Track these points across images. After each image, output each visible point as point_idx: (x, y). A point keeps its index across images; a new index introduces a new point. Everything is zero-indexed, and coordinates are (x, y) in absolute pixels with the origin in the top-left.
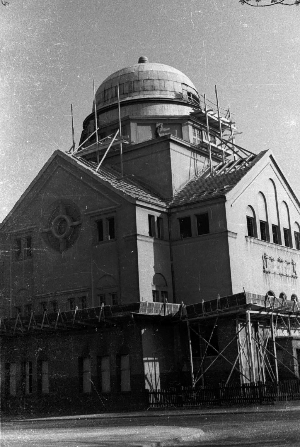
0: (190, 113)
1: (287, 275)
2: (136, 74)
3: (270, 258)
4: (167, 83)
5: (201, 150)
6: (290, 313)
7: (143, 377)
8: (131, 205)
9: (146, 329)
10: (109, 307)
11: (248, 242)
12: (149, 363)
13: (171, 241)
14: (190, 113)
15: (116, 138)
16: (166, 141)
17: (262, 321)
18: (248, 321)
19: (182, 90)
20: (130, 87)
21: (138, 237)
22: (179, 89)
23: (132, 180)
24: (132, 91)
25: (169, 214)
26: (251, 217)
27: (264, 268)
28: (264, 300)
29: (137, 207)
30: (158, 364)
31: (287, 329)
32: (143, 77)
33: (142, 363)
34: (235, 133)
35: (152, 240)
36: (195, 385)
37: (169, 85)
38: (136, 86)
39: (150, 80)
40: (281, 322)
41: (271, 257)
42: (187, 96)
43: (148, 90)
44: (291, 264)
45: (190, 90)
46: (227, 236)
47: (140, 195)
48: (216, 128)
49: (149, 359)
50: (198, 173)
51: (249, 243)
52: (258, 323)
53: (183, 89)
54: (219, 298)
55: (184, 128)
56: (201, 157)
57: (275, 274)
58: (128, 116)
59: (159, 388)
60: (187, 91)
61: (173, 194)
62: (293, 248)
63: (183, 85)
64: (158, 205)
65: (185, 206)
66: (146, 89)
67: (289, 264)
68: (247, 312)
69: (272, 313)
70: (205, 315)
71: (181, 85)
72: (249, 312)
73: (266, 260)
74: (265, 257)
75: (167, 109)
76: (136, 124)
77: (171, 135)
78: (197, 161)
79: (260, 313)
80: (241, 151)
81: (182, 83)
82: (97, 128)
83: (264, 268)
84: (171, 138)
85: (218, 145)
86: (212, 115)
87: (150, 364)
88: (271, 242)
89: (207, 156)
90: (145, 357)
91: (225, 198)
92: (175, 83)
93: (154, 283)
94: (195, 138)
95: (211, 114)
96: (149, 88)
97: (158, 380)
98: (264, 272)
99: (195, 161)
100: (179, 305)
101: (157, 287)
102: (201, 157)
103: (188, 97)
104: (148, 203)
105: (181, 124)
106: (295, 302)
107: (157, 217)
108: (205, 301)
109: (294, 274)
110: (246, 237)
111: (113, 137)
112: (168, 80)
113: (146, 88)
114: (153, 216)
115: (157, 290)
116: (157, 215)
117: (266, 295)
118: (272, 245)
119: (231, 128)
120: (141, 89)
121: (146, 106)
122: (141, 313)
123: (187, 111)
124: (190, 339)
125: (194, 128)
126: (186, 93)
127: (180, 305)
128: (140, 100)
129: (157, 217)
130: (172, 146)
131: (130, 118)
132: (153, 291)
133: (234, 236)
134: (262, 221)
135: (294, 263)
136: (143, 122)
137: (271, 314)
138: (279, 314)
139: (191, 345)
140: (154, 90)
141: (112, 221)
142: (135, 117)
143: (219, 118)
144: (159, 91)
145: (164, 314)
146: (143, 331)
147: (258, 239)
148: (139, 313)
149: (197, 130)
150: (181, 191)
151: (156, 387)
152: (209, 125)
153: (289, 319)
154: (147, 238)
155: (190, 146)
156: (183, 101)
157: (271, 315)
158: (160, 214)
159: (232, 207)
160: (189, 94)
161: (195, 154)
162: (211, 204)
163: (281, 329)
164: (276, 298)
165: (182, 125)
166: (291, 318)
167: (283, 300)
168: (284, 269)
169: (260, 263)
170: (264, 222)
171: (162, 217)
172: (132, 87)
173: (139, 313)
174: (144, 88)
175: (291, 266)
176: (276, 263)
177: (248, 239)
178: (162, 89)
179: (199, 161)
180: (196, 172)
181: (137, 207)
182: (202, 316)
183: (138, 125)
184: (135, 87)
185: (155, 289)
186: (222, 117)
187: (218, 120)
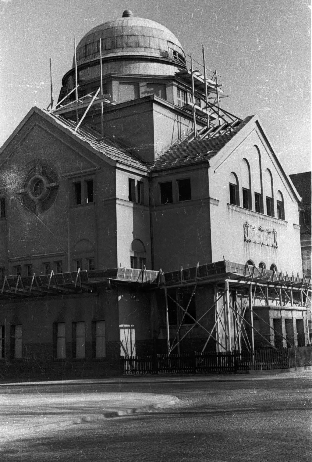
4: (152, 39)
6: (269, 283)
10: (86, 272)
13: (151, 206)
16: (150, 101)
17: (239, 290)
20: (113, 42)
21: (117, 202)
22: (165, 47)
25: (149, 179)
27: (245, 237)
29: (117, 170)
30: (133, 331)
31: (265, 299)
35: (132, 205)
37: (154, 43)
40: (259, 292)
42: (173, 55)
43: (131, 47)
44: (272, 233)
48: (201, 90)
51: (230, 211)
52: (237, 292)
55: (168, 89)
56: (185, 120)
57: (255, 243)
58: (110, 74)
59: (134, 355)
68: (226, 280)
72: (228, 281)
74: (246, 226)
81: (169, 41)
83: (245, 237)
84: (155, 99)
86: (198, 76)
87: (126, 331)
89: (191, 119)
91: (208, 163)
92: (161, 41)
96: (133, 45)
98: (245, 240)
100: (157, 272)
101: (135, 253)
102: (185, 120)
104: (129, 166)
106: (274, 272)
108: (184, 269)
111: (94, 95)
112: (153, 37)
116: (137, 178)
118: (254, 214)
120: (125, 45)
122: (118, 279)
123: (172, 71)
124: (167, 306)
125: (179, 89)
130: (155, 107)
132: (131, 257)
136: (126, 80)
139: (167, 313)
140: (139, 47)
141: (90, 184)
143: (205, 80)
144: (143, 48)
145: (141, 281)
146: (120, 298)
148: (116, 278)
151: (132, 354)
158: (141, 178)
160: (175, 53)
161: (179, 116)
167: (263, 269)
173: (117, 279)
175: (272, 235)
177: (230, 207)
179: (182, 124)
180: (179, 135)
181: (117, 170)
185: (133, 255)
187: (204, 82)
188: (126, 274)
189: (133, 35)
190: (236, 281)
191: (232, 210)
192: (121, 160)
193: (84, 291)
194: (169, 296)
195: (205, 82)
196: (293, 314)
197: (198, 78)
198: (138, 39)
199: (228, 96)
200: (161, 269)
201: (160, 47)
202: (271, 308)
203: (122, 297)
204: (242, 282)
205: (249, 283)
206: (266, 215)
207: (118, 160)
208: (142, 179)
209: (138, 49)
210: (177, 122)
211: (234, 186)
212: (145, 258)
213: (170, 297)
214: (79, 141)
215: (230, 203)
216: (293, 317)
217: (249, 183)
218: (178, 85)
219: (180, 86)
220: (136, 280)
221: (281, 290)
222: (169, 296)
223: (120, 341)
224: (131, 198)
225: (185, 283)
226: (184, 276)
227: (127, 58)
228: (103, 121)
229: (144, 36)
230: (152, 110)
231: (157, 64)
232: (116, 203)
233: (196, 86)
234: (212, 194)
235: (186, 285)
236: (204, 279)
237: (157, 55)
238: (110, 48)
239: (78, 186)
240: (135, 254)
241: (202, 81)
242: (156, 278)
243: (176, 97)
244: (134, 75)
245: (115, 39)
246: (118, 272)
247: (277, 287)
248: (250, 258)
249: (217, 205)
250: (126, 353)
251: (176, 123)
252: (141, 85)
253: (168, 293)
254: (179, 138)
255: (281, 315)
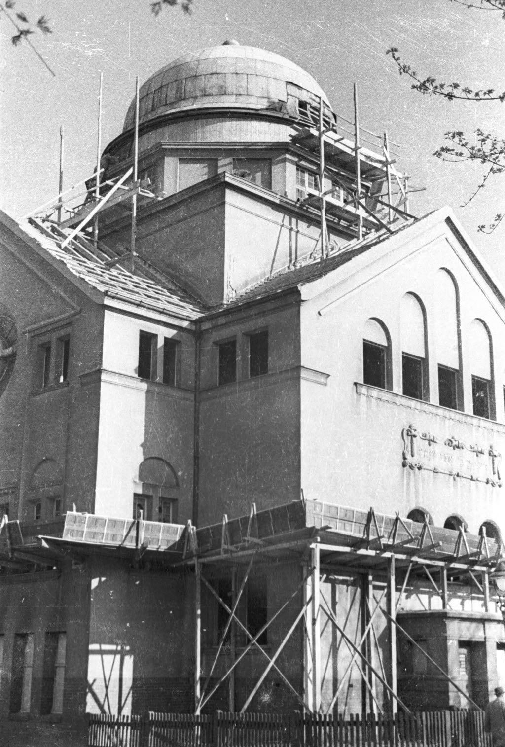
0: (291, 138)
1: (472, 476)
2: (193, 65)
3: (425, 436)
4: (253, 79)
5: (307, 211)
6: (449, 559)
7: (80, 686)
8: (90, 308)
9: (103, 579)
10: (16, 523)
11: (362, 396)
12: (105, 657)
13: (198, 391)
14: (291, 138)
15: (124, 184)
16: (216, 187)
17: (357, 568)
18: (314, 568)
19: (286, 94)
20: (178, 90)
21: (104, 376)
22: (279, 93)
23: (158, 271)
24: (181, 97)
25: (196, 332)
26: (484, 379)
27: (405, 458)
28: (365, 522)
29: (106, 312)
30: (129, 661)
31: (438, 594)
32: (203, 69)
33: (88, 652)
34: (411, 189)
35: (144, 386)
36: (202, 711)
37: (257, 86)
38: (189, 87)
39: (219, 74)
40: (417, 577)
41: (428, 435)
42: (298, 109)
43: (211, 95)
44: (486, 453)
45: (305, 97)
46: (298, 378)
47: (115, 287)
48: (342, 167)
49: (105, 647)
50: (299, 259)
51: (363, 399)
52: (370, 578)
53: (288, 95)
54: (254, 511)
55: (276, 169)
56: (308, 227)
57: (436, 472)
58: (160, 142)
59: (127, 711)
60: (298, 98)
61: (225, 297)
62: (431, 400)
63: (289, 86)
64: (165, 311)
65: (225, 315)
66: (207, 93)
67: (479, 454)
68: (313, 546)
69: (392, 554)
70: (226, 551)
71: (285, 86)
72: (317, 547)
73: (412, 440)
74: (409, 433)
75: (246, 130)
76: (176, 159)
77: (226, 174)
78: (299, 235)
79: (355, 551)
80: (403, 217)
81: (288, 83)
82: (101, 169)
83: (405, 458)
84: (227, 180)
85: (325, 194)
86: (336, 141)
87: (108, 658)
88: (431, 403)
89: (315, 222)
90: (93, 643)
91: (298, 293)
92: (273, 82)
93: (141, 477)
94: (301, 188)
95: (336, 139)
96: (215, 91)
97: (127, 697)
98: (404, 465)
99: (294, 234)
100: (180, 527)
101: (144, 486)
102: (308, 227)
103: (299, 110)
104: (139, 305)
105: (270, 159)
106: (460, 535)
107: (166, 339)
108: (231, 520)
109: (494, 478)
110: (356, 384)
111: (116, 182)
112: (257, 75)
113: (208, 91)
114: (155, 336)
115: (146, 492)
116: (163, 333)
117: (369, 510)
118: (434, 410)
119: (387, 172)
120: (199, 93)
121: (203, 126)
122: (67, 537)
123: (283, 134)
124: (198, 605)
125: (300, 168)
126: (296, 101)
127: (184, 526)
128: (190, 113)
129: (166, 339)
130: (231, 197)
131: (163, 147)
132: (136, 495)
133: (322, 380)
134: (368, 341)
135: (495, 453)
136: (188, 156)
137: (390, 556)
138: (415, 558)
139: (199, 621)
140: (225, 94)
141: (66, 342)
142: (174, 145)
143: (355, 150)
144: (235, 96)
145: (135, 544)
146: (95, 583)
147: (466, 412)
148: (61, 537)
149: (309, 174)
150: (247, 291)
151: (120, 708)
152: (325, 160)
153: (445, 572)
154: (131, 380)
155: (278, 202)
156: (280, 115)
157: (389, 560)
158: (174, 332)
159: (321, 317)
160: (303, 104)
161: (294, 220)
162: (274, 309)
163: (460, 597)
164: (401, 521)
165: (273, 161)
166: (450, 570)
167: (425, 526)
168: (466, 464)
169: (395, 446)
170: (420, 358)
171: (178, 339)
172: (181, 90)
173: (63, 539)
174: (205, 91)
175: (486, 457)
176: (440, 448)
177: (364, 390)
178: (242, 93)
179: (302, 234)
180: (294, 257)
181: (106, 312)
182: (219, 554)
183: (182, 161)
184: (188, 89)
185: (140, 491)
186: (361, 148)
187: (353, 154)
188: (89, 527)
189: (216, 74)
190: (347, 549)
191: (369, 397)
192: (113, 291)
193: (40, 569)
194: (204, 580)
195: (356, 153)
196: (486, 631)
197: (337, 145)
198: (225, 81)
199: (424, 189)
200: (190, 521)
201: (269, 93)
202: (448, 615)
203: (100, 580)
204: (362, 552)
205: (387, 554)
206: (471, 413)
207: (107, 291)
208: (177, 334)
209: (225, 98)
210: (288, 231)
211: (485, 384)
212: (177, 500)
213: (207, 584)
214: (49, 260)
215: (362, 382)
216: (485, 638)
217: (423, 346)
218: (300, 160)
219: (303, 163)
220: (120, 543)
221: (487, 576)
222: (204, 580)
223: (87, 682)
224: (144, 371)
225: (232, 552)
226: (232, 536)
227: (198, 115)
228: (135, 230)
229: (237, 74)
230: (224, 203)
231: (258, 122)
232: (99, 380)
233: (328, 157)
234: (309, 355)
235: (234, 555)
236: (270, 543)
237: (260, 105)
238: (173, 100)
239: (46, 348)
240: (143, 490)
241: (349, 151)
242: (177, 539)
243: (290, 181)
244: (210, 144)
245: (182, 83)
246: (65, 523)
247: (477, 568)
248: (417, 503)
249: (326, 384)
250: (101, 707)
251: (285, 232)
252: (220, 163)
253: (202, 574)
254: (291, 261)
255: (485, 633)
